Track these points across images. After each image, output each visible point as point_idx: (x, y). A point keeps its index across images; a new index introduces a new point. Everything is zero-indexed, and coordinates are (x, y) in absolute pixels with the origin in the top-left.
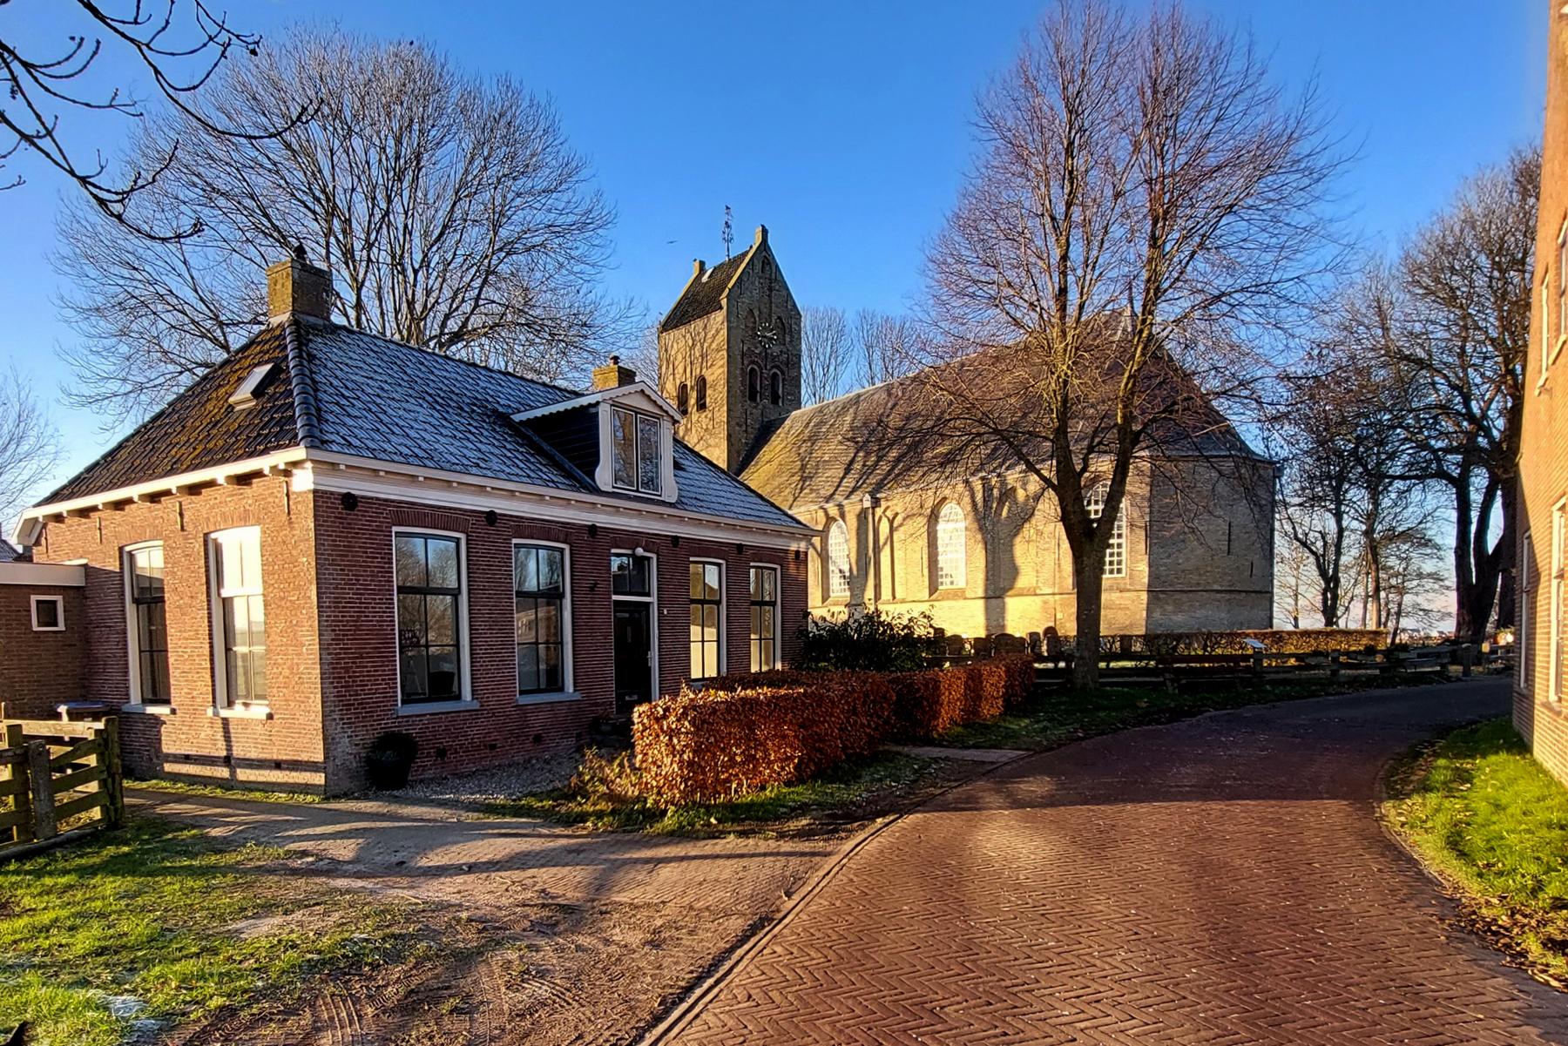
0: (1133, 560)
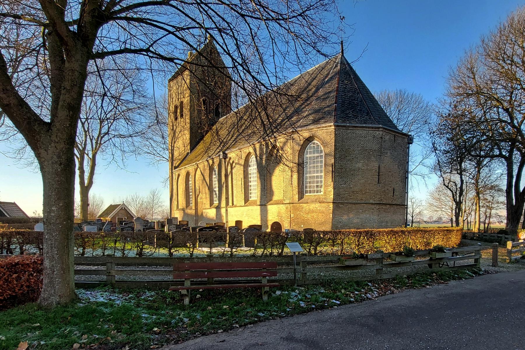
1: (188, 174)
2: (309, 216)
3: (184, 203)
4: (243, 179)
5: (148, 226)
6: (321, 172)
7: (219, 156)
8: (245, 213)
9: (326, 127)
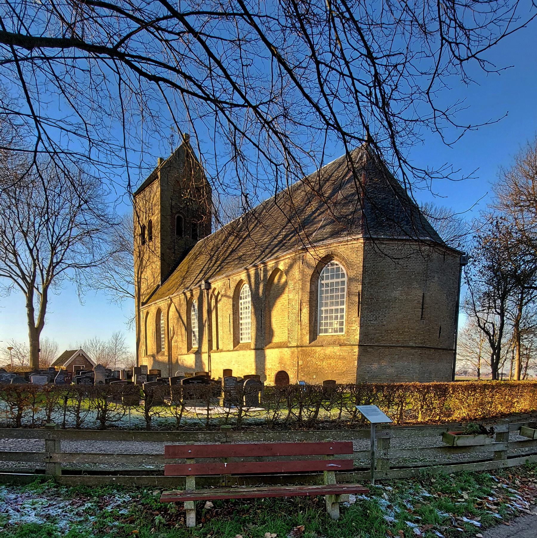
0: (349, 323)
1: (159, 311)
2: (324, 364)
3: (155, 347)
4: (232, 316)
5: (111, 376)
6: (342, 303)
7: (200, 286)
8: (234, 360)
9: (351, 240)
